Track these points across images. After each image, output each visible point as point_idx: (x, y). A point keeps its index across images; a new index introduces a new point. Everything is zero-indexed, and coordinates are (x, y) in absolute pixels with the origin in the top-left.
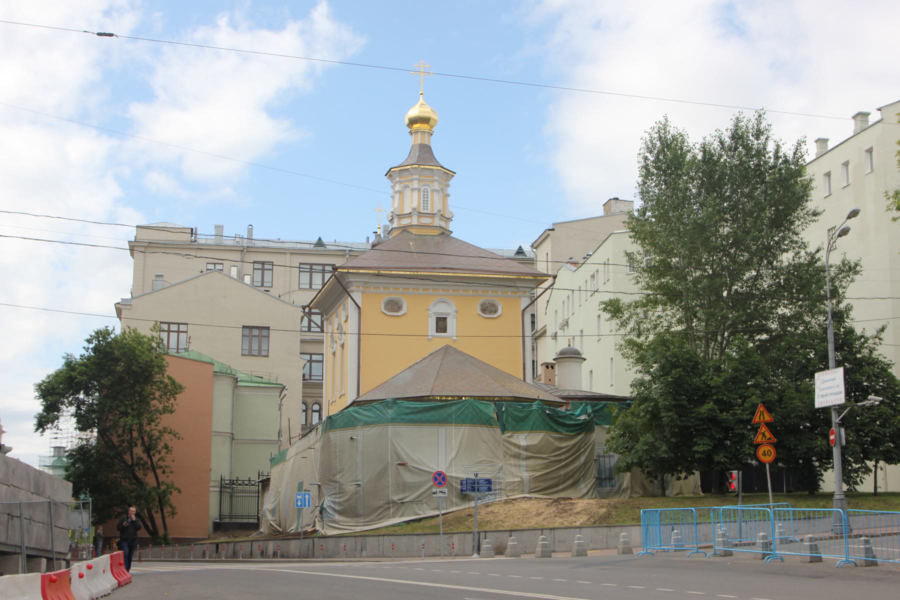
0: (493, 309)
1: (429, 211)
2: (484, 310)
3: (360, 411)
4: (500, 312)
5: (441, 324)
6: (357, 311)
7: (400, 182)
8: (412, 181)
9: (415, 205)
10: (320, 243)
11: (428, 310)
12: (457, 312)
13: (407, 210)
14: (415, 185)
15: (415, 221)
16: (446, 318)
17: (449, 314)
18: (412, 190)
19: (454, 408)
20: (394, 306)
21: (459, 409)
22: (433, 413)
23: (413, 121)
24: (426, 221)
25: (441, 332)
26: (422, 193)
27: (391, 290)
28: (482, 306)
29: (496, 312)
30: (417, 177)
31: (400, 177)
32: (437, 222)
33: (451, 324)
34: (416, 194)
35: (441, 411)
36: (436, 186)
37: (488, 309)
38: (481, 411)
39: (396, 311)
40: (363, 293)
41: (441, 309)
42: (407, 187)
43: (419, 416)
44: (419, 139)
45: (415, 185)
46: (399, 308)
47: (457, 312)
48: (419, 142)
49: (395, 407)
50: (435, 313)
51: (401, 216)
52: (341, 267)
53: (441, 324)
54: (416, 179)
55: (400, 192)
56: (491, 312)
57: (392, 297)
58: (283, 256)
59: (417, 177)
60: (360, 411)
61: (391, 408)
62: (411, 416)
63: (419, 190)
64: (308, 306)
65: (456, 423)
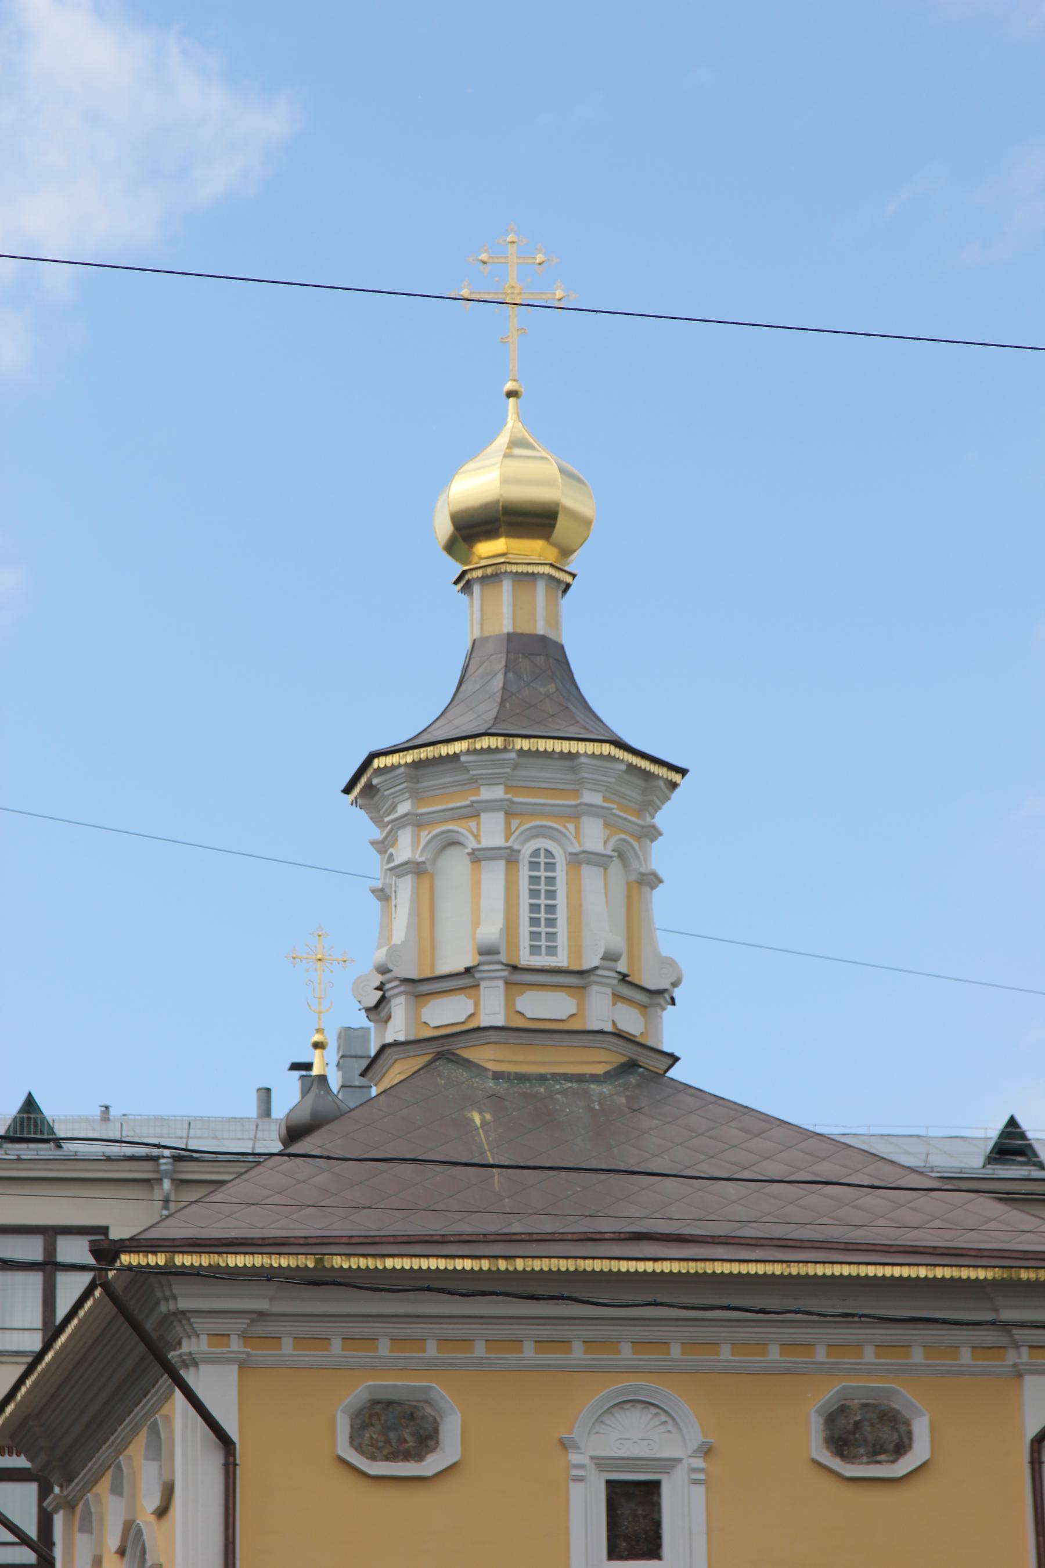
0: (886, 1434)
1: (561, 960)
4: (920, 1452)
6: (216, 1459)
7: (418, 822)
8: (473, 812)
9: (491, 930)
11: (565, 1445)
12: (707, 1451)
13: (454, 957)
14: (492, 831)
15: (491, 1007)
16: (652, 1488)
17: (669, 1464)
18: (478, 857)
20: (396, 1429)
23: (472, 527)
24: (545, 1006)
26: (524, 873)
27: (384, 1348)
28: (831, 1419)
29: (901, 1448)
30: (497, 792)
31: (417, 796)
32: (601, 1010)
34: (494, 876)
36: (593, 836)
37: (864, 1434)
40: (244, 1366)
41: (633, 1439)
42: (453, 842)
44: (503, 613)
45: (492, 831)
46: (426, 1440)
47: (707, 1451)
48: (507, 627)
50: (601, 1463)
51: (423, 987)
52: (133, 1245)
54: (491, 806)
55: (417, 870)
56: (876, 1452)
57: (152, 1519)
59: (497, 792)
63: (511, 857)
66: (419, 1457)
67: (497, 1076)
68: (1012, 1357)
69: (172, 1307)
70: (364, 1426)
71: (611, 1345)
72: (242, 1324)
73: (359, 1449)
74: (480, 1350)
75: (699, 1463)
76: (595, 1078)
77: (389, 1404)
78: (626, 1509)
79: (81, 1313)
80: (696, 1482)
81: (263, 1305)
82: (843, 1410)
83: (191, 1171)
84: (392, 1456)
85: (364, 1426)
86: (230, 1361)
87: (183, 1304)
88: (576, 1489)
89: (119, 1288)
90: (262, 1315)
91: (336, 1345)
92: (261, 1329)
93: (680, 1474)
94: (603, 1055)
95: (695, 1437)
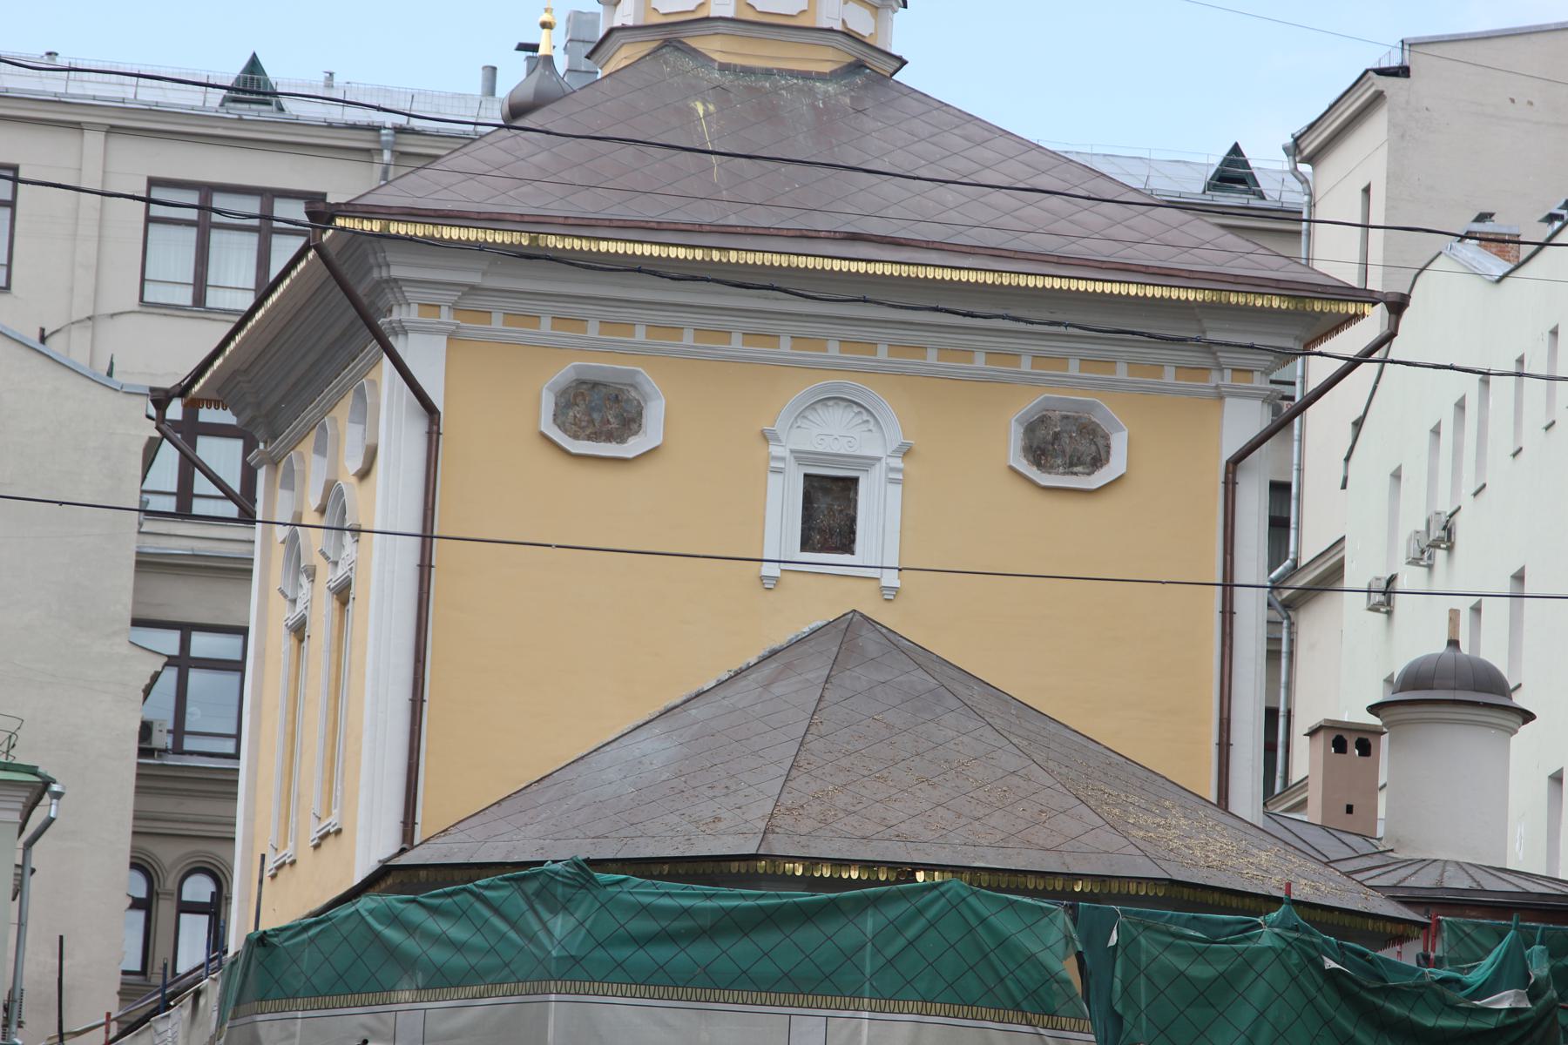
0: (1085, 447)
2: (1039, 453)
3: (416, 915)
4: (1116, 466)
5: (829, 513)
6: (420, 427)
10: (252, 85)
11: (766, 437)
12: (906, 452)
17: (868, 462)
19: (870, 923)
20: (601, 410)
21: (898, 927)
22: (768, 939)
25: (813, 550)
27: (593, 329)
28: (1030, 429)
29: (1098, 461)
33: (878, 513)
35: (808, 936)
37: (1064, 445)
38: (1003, 942)
39: (609, 437)
40: (452, 337)
41: (834, 436)
43: (701, 952)
46: (628, 422)
47: (906, 452)
49: (585, 906)
50: (801, 457)
53: (829, 513)
56: (1073, 463)
57: (354, 480)
58: (67, 139)
60: (416, 915)
61: (564, 907)
62: (662, 953)
64: (183, 391)
65: (877, 994)
66: (622, 440)
67: (724, 67)
68: (1215, 378)
69: (384, 274)
70: (569, 405)
71: (819, 343)
72: (452, 296)
73: (562, 427)
74: (688, 338)
75: (897, 463)
76: (821, 77)
77: (595, 385)
78: (822, 503)
79: (294, 274)
80: (893, 481)
81: (475, 279)
82: (1043, 420)
83: (411, 145)
84: (594, 437)
85: (569, 405)
86: (439, 332)
87: (396, 272)
88: (774, 481)
89: (332, 252)
90: (473, 289)
91: (546, 324)
92: (470, 303)
93: (878, 471)
94: (830, 54)
95: (896, 437)
